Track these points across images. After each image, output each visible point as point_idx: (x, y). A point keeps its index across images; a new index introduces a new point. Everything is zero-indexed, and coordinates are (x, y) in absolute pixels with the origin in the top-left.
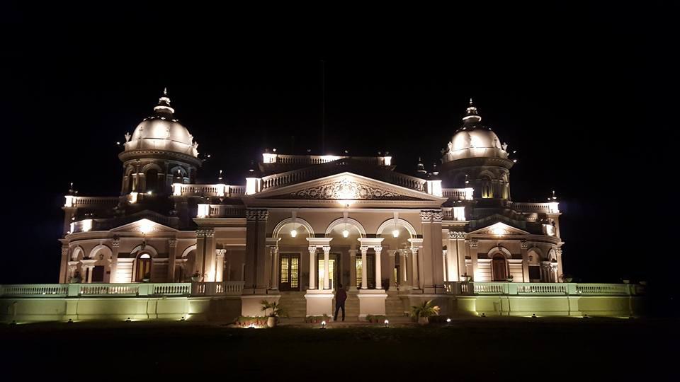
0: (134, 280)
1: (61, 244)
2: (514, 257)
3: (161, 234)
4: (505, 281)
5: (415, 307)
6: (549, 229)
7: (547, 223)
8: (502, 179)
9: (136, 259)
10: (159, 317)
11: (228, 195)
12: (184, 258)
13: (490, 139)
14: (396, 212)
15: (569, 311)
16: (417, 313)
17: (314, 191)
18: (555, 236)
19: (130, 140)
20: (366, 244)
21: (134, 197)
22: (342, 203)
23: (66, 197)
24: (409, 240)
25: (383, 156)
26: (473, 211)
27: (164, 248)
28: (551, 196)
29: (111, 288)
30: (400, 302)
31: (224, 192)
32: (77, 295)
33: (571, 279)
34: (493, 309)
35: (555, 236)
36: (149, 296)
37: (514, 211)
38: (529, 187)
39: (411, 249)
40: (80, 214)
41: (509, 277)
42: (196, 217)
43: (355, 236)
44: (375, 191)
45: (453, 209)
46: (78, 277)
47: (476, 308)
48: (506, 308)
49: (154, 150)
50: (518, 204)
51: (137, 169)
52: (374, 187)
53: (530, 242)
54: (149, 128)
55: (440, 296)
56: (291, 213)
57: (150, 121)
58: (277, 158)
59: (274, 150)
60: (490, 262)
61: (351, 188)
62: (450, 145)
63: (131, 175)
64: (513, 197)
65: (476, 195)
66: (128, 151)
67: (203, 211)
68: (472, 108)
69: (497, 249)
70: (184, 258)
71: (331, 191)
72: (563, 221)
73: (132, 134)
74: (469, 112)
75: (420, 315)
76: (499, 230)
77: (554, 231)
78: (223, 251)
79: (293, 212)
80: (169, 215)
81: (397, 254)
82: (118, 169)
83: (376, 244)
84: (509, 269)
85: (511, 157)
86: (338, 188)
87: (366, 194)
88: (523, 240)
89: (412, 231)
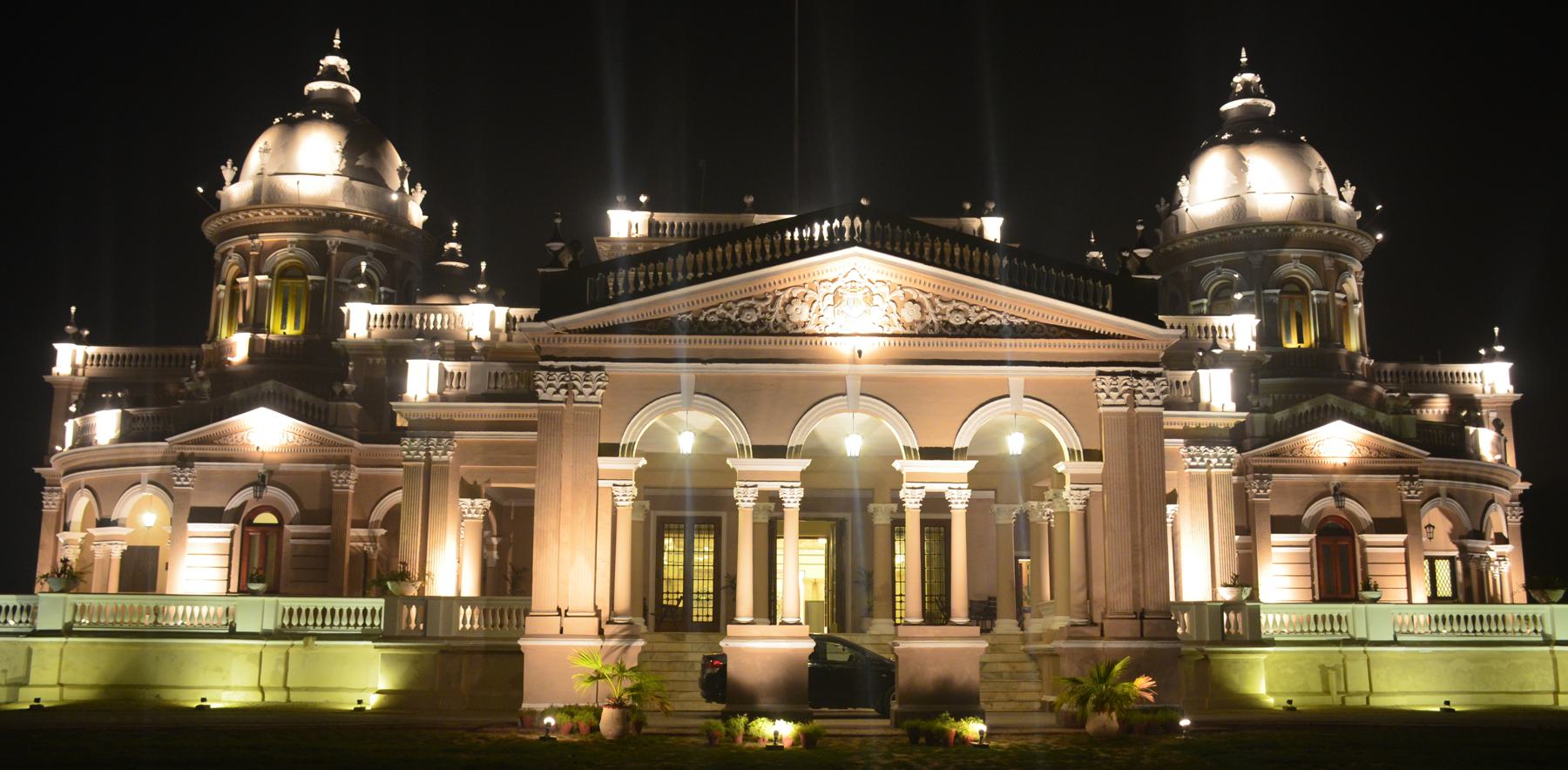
0: (234, 588)
1: (40, 482)
2: (1382, 526)
3: (311, 454)
4: (1356, 600)
5: (1075, 681)
6: (1486, 440)
7: (1479, 423)
8: (1342, 291)
9: (238, 527)
10: (296, 697)
11: (503, 337)
12: (376, 525)
13: (1307, 170)
14: (1016, 377)
15: (1556, 693)
16: (1083, 701)
17: (751, 307)
18: (1503, 462)
19: (236, 180)
20: (921, 479)
21: (239, 346)
22: (843, 348)
23: (56, 346)
24: (1060, 467)
25: (979, 216)
26: (1257, 384)
27: (313, 494)
28: (1489, 342)
29: (172, 609)
30: (1030, 666)
31: (492, 328)
32: (59, 627)
33: (1560, 593)
34: (1317, 687)
35: (1503, 462)
36: (266, 635)
37: (1378, 388)
38: (1421, 322)
39: (1065, 495)
40: (92, 395)
41: (1367, 587)
42: (401, 399)
43: (714, 454)
44: (949, 307)
45: (1196, 378)
46: (70, 579)
47: (1269, 684)
48: (1358, 683)
49: (298, 208)
50: (1390, 367)
51: (253, 263)
52: (948, 296)
53: (1429, 482)
54: (286, 145)
55: (1157, 645)
56: (677, 380)
57: (291, 124)
58: (653, 226)
59: (643, 199)
60: (1309, 545)
61: (870, 297)
62: (1184, 187)
63: (235, 283)
64: (1376, 342)
65: (1268, 336)
66: (228, 213)
67: (422, 380)
68: (1249, 77)
69: (1328, 503)
70: (376, 525)
71: (806, 308)
72: (1525, 419)
73: (239, 163)
74: (1239, 88)
75: (1090, 705)
76: (1337, 443)
77: (1500, 447)
78: (482, 504)
79: (684, 377)
80: (330, 396)
81: (1024, 518)
82: (201, 267)
83: (952, 480)
84: (1365, 563)
85: (1367, 225)
86: (829, 299)
87: (918, 316)
88: (1409, 474)
89: (1067, 439)
